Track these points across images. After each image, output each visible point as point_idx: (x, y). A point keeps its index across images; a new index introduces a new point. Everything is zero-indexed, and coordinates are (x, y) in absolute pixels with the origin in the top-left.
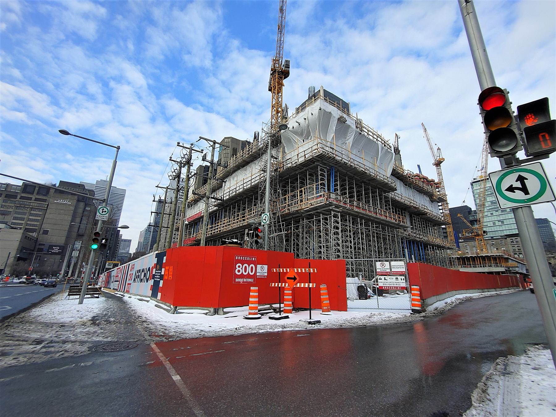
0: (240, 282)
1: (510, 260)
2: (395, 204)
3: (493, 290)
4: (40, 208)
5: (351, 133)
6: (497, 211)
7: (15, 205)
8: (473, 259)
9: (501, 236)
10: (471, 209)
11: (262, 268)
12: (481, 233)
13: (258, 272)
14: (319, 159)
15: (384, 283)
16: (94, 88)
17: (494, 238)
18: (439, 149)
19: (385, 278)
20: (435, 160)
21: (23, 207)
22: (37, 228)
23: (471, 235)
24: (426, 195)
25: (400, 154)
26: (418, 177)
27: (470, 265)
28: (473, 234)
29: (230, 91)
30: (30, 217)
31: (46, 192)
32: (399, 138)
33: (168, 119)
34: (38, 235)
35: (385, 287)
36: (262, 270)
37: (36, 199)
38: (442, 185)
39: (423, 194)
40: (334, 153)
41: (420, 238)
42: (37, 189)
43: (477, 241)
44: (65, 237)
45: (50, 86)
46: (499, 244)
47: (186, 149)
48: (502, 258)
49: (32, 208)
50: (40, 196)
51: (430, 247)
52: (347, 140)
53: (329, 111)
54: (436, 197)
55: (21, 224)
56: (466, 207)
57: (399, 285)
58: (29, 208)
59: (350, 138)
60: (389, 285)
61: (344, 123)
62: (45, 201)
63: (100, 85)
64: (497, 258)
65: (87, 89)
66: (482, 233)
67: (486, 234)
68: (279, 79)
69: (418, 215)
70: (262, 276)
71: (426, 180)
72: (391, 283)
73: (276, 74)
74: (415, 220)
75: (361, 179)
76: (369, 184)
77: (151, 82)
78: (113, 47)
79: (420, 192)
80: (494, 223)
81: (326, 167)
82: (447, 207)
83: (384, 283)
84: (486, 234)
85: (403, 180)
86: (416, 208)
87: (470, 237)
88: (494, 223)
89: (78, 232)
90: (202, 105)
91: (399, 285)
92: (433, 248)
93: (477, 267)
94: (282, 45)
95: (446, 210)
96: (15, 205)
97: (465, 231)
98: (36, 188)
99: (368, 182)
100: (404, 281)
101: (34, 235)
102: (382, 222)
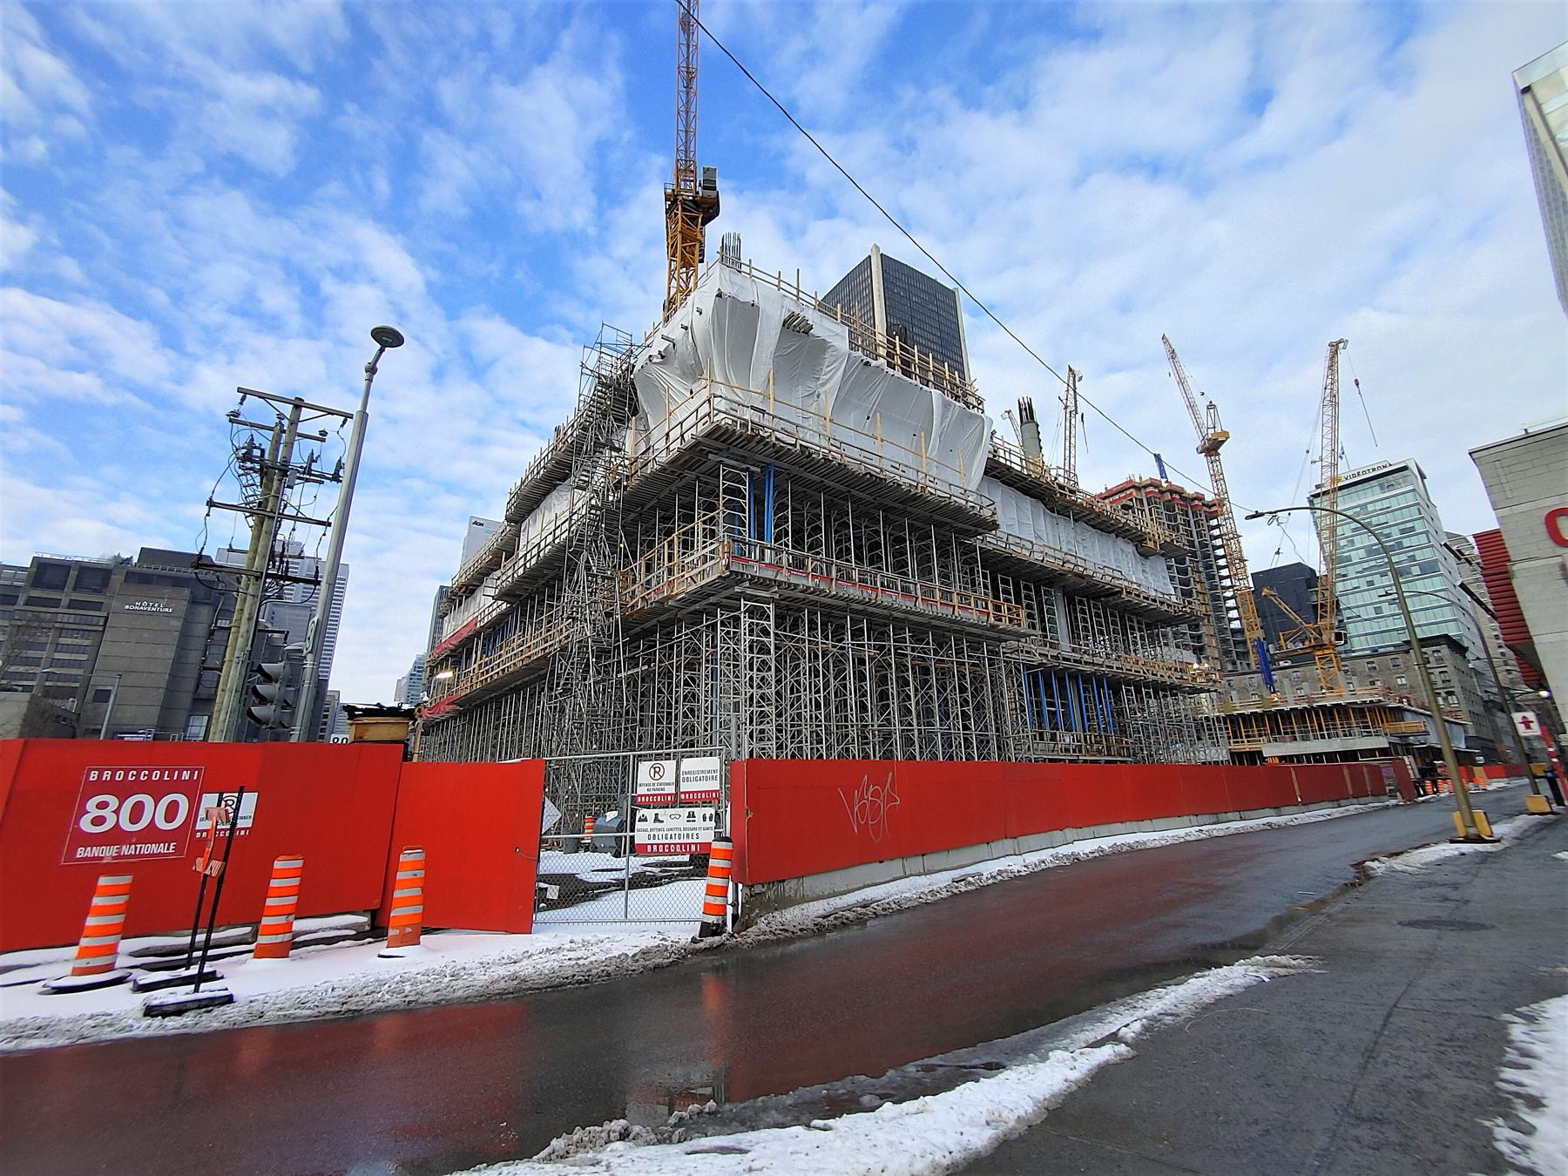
0: (102, 858)
1: (1407, 713)
2: (1012, 569)
3: (1272, 811)
4: (85, 627)
5: (835, 362)
6: (1383, 575)
7: (15, 623)
8: (1300, 714)
9: (1394, 646)
10: (1313, 571)
11: (657, 770)
12: (1330, 639)
13: (640, 786)
14: (719, 445)
15: (652, 834)
16: (278, 298)
17: (1380, 650)
18: (1211, 406)
19: (656, 815)
20: (1201, 438)
21: (36, 628)
22: (77, 685)
23: (1301, 646)
24: (1124, 538)
25: (1035, 422)
26: (1156, 487)
27: (1293, 733)
28: (1307, 643)
29: (644, 288)
30: (58, 656)
31: (100, 582)
32: (1080, 379)
33: (477, 370)
34: (80, 704)
35: (652, 845)
36: (657, 776)
37: (73, 604)
38: (1225, 507)
39: (1113, 535)
40: (767, 424)
41: (1093, 664)
42: (73, 573)
43: (1319, 666)
44: (159, 708)
45: (158, 297)
46: (1390, 669)
47: (261, 431)
48: (1384, 708)
49: (62, 629)
50: (83, 593)
51: (1128, 691)
52: (823, 385)
53: (749, 299)
54: (1155, 542)
55: (32, 676)
56: (1299, 567)
57: (695, 836)
58: (52, 631)
59: (833, 374)
60: (666, 839)
61: (807, 333)
62: (98, 606)
63: (298, 290)
64: (1366, 710)
65: (260, 301)
66: (1333, 639)
67: (1343, 642)
68: (688, 224)
69: (1096, 597)
70: (657, 795)
71: (1177, 497)
72: (673, 833)
73: (678, 210)
74: (1082, 611)
75: (875, 499)
76: (903, 513)
77: (434, 275)
78: (334, 188)
79: (1102, 530)
80: (1378, 610)
81: (748, 468)
82: (1243, 570)
83: (652, 834)
84: (1343, 642)
85: (1043, 497)
86: (1084, 578)
87: (1300, 652)
88: (1378, 610)
89: (196, 691)
90: (570, 327)
91: (695, 836)
92: (1138, 691)
93: (1312, 737)
94: (693, 125)
95: (1239, 580)
96: (15, 623)
97: (1283, 635)
98: (71, 573)
99: (901, 506)
100: (713, 824)
101: (71, 704)
102: (934, 622)
